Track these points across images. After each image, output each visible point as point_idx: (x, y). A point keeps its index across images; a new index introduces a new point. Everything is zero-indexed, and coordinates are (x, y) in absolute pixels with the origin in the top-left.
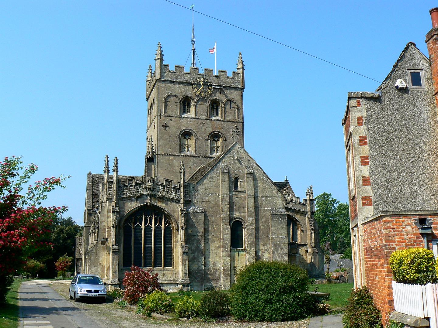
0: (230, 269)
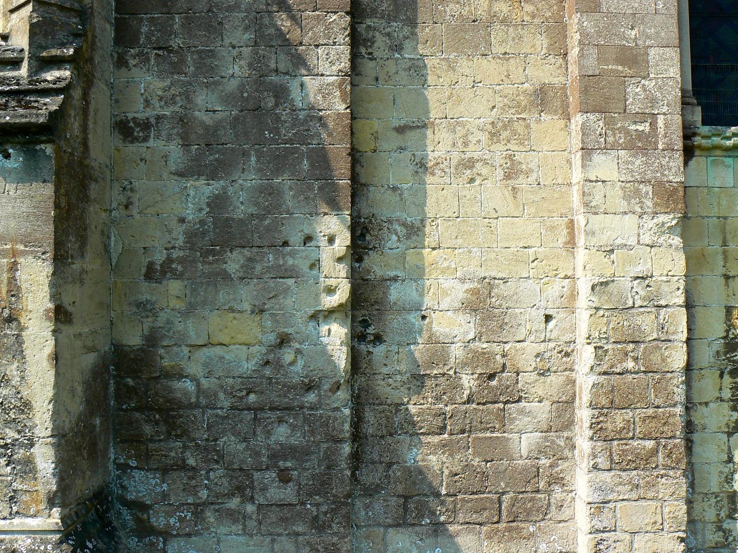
0: (678, 359)
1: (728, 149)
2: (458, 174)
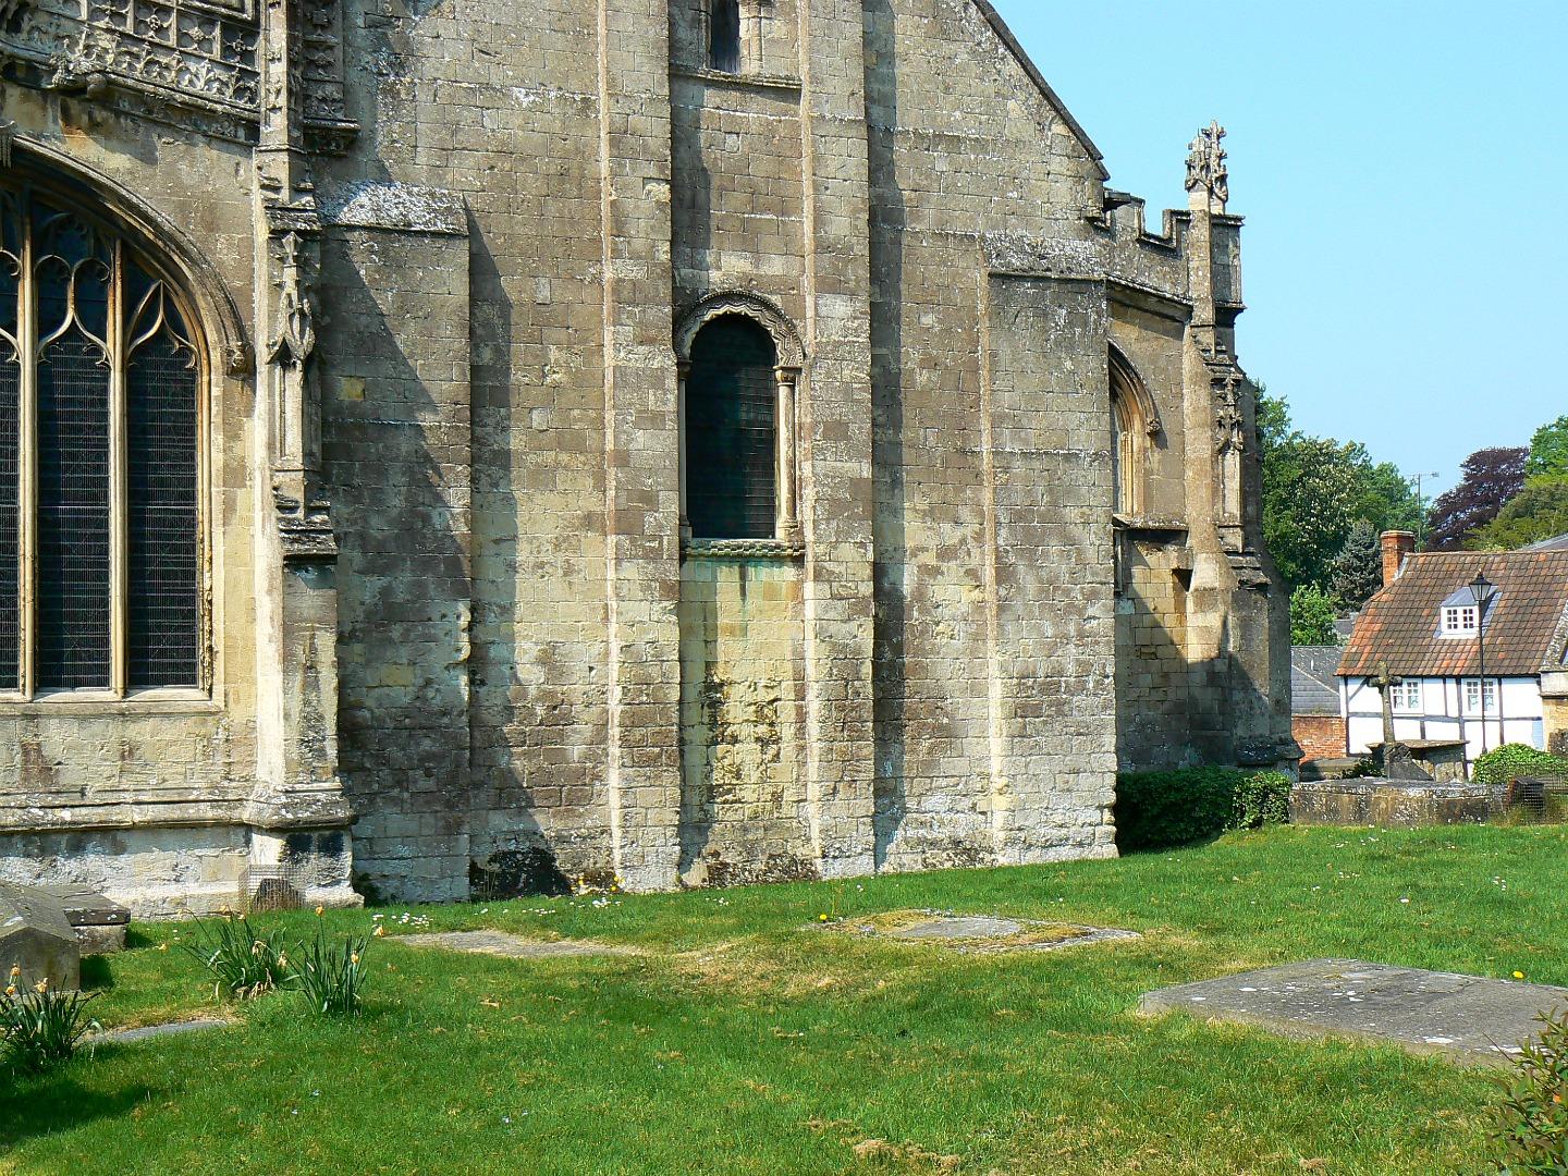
0: (675, 695)
1: (708, 556)
2: (533, 573)
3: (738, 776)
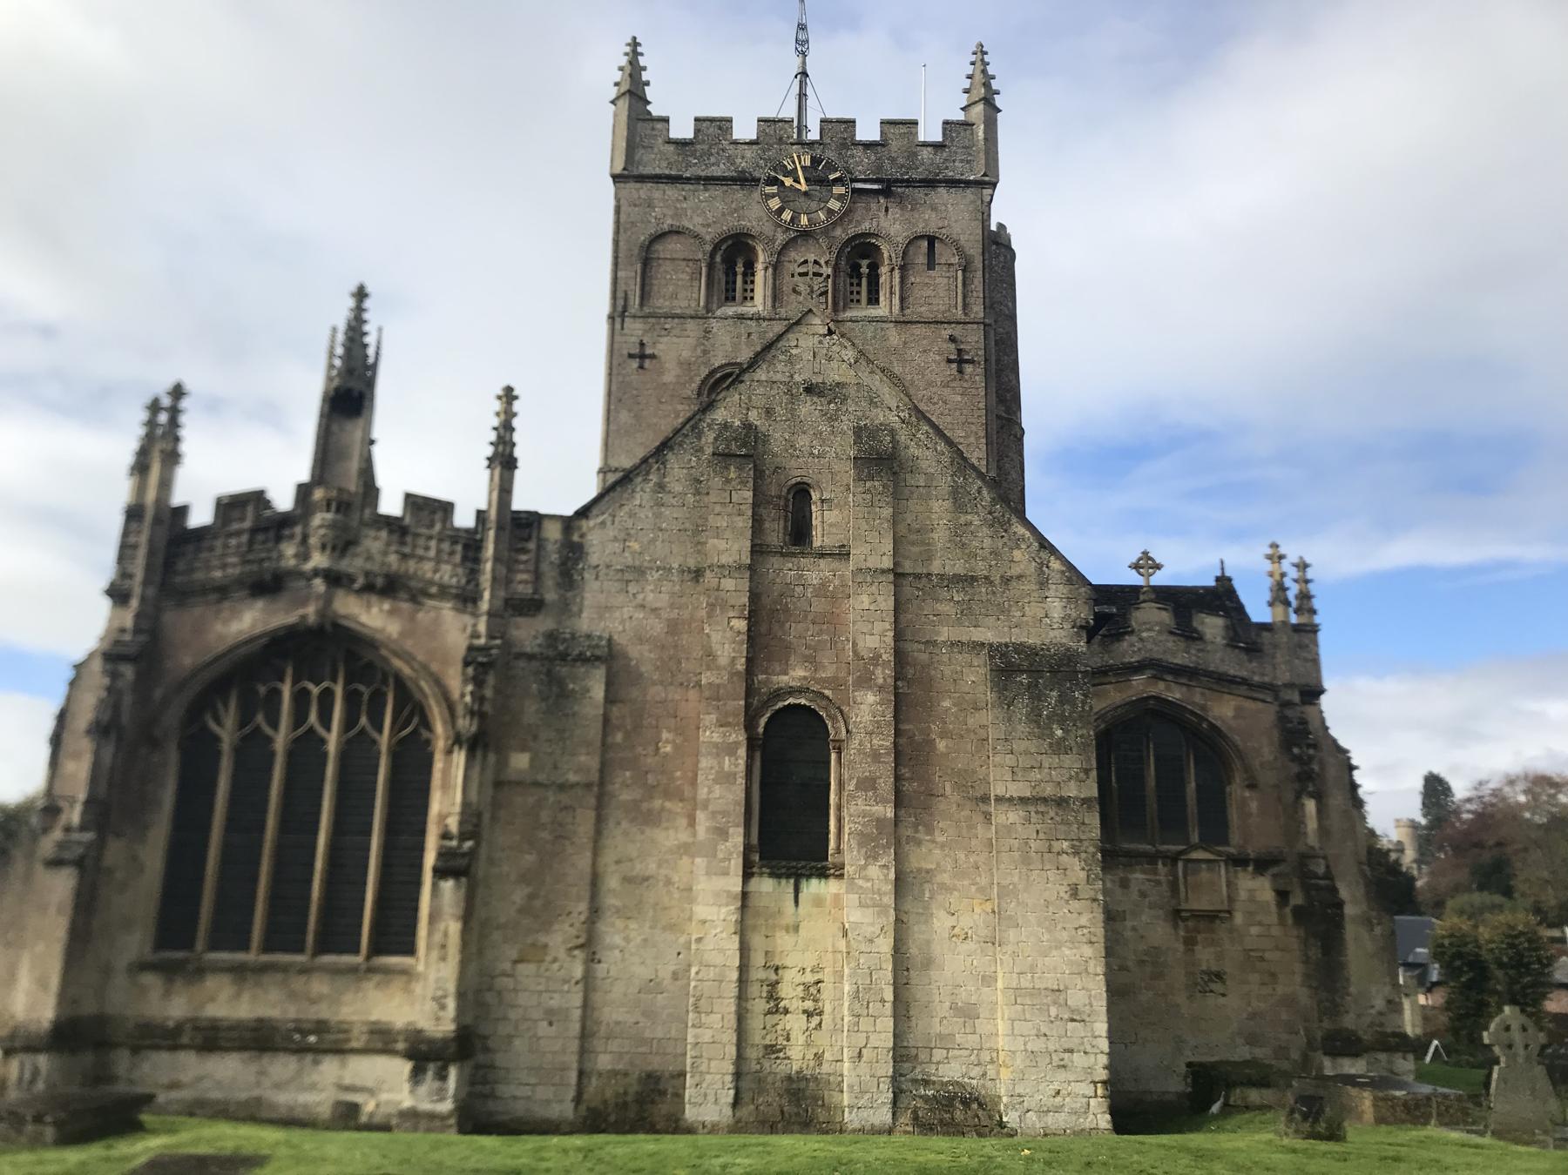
3: (788, 1039)
